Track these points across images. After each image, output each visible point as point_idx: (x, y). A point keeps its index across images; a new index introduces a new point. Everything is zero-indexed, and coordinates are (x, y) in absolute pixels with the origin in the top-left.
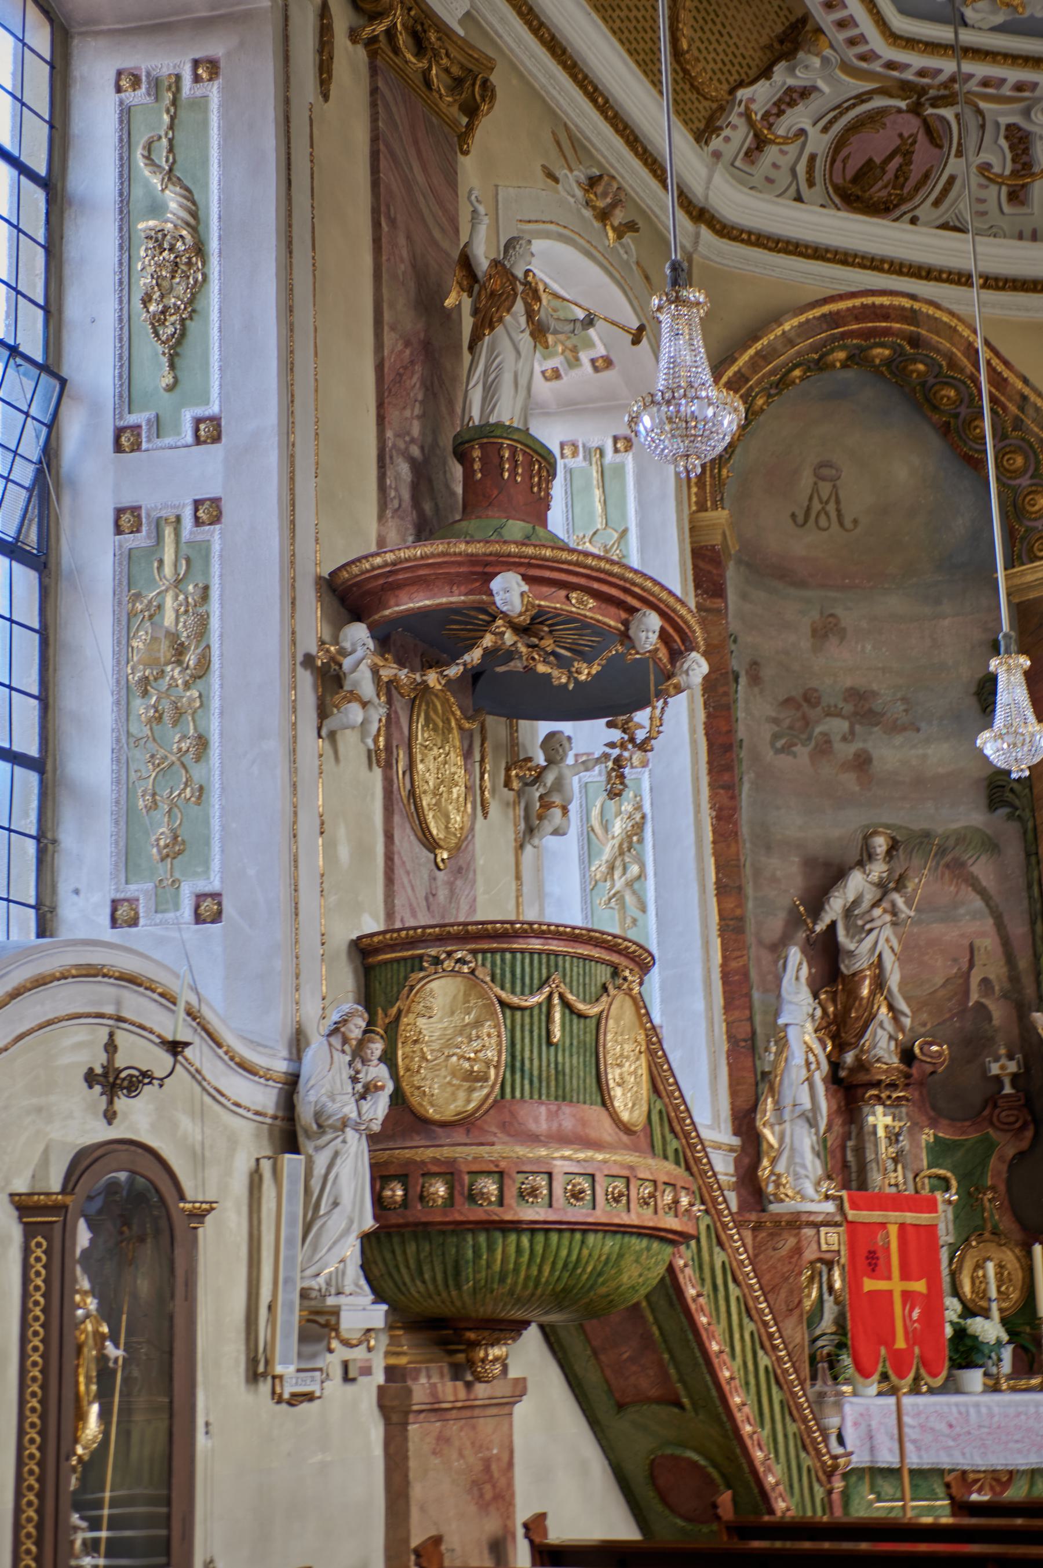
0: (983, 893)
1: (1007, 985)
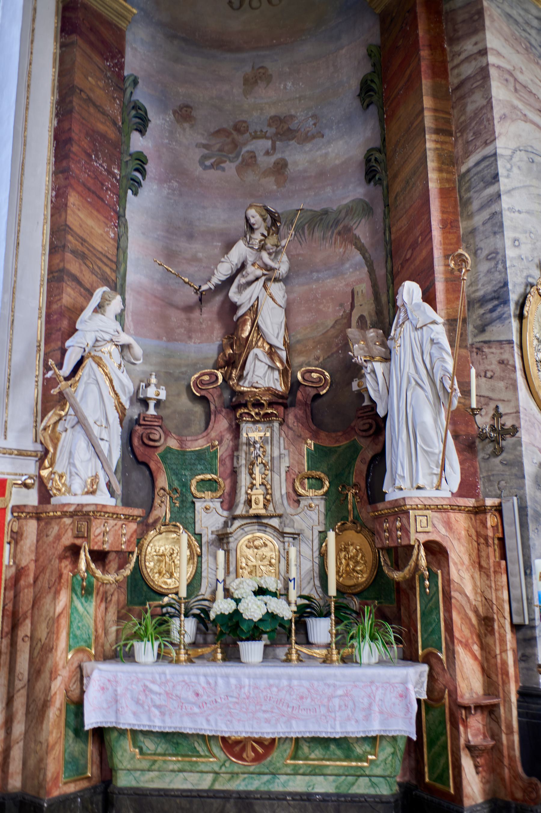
0: (362, 249)
1: (375, 318)
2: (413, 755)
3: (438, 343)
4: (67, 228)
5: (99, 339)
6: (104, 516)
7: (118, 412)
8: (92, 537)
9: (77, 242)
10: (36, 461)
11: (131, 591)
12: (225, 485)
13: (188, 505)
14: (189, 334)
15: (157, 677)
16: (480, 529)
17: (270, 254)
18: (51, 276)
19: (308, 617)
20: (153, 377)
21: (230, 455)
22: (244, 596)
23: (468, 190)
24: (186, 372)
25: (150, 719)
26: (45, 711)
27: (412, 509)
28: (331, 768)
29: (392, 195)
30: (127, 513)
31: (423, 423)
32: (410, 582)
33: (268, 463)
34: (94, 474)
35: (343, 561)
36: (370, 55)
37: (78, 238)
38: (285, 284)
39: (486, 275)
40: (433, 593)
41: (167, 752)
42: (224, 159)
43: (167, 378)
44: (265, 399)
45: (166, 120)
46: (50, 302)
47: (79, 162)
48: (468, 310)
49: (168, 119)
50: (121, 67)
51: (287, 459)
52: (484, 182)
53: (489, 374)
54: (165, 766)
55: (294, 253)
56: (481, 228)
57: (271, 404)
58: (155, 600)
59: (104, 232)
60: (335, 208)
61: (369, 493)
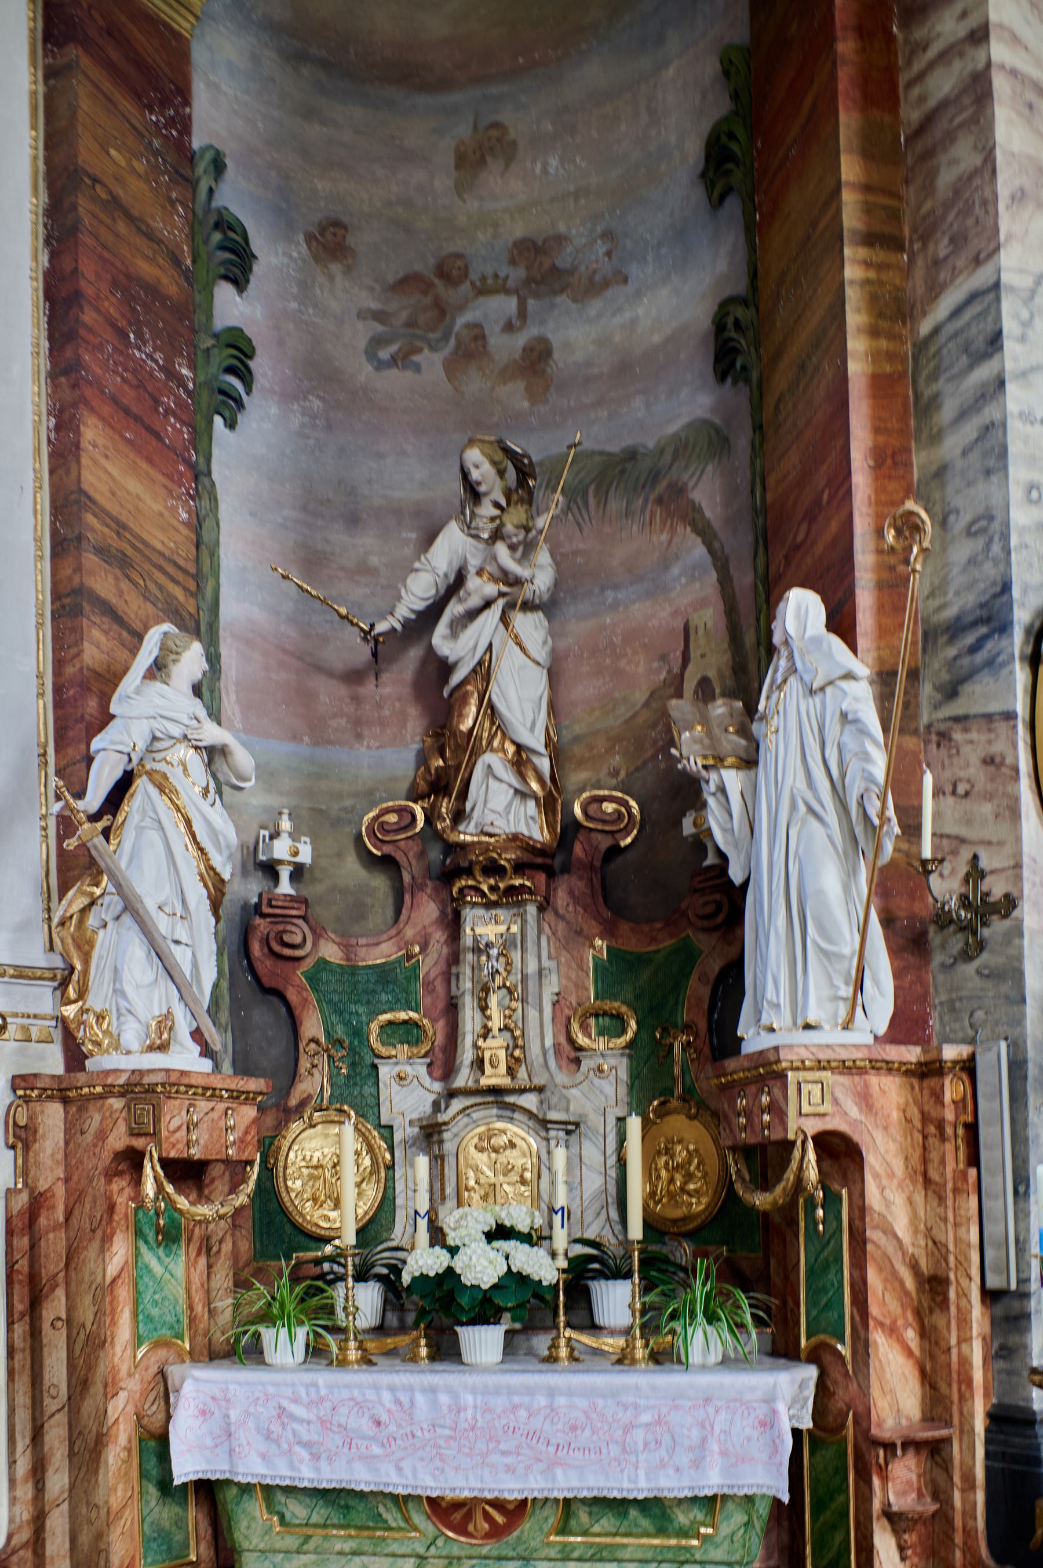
0: (705, 532)
1: (730, 682)
2: (785, 1524)
3: (856, 721)
4: (83, 499)
5: (158, 734)
6: (187, 1092)
7: (206, 886)
8: (164, 1134)
9: (106, 530)
10: (55, 989)
11: (261, 1234)
12: (436, 1031)
13: (365, 1071)
14: (358, 728)
15: (303, 1392)
16: (929, 1106)
17: (512, 548)
18: (58, 604)
19: (593, 1278)
20: (285, 817)
21: (443, 973)
22: (466, 1241)
23: (934, 377)
24: (353, 808)
25: (292, 1466)
26: (100, 1452)
27: (792, 1069)
28: (630, 1549)
29: (770, 401)
30: (233, 1087)
31: (820, 892)
32: (788, 1211)
33: (516, 986)
34: (165, 1011)
35: (664, 1173)
36: (726, 73)
37: (108, 520)
38: (549, 616)
39: (964, 570)
40: (831, 1232)
41: (329, 1522)
42: (419, 344)
43: (313, 820)
44: (507, 858)
45: (291, 257)
46: (59, 661)
47: (100, 348)
48: (924, 650)
49: (295, 255)
50: (185, 126)
51: (554, 978)
52: (969, 355)
53: (961, 789)
54: (326, 1545)
55: (566, 548)
56: (959, 464)
57: (519, 868)
58: (308, 1249)
59: (166, 508)
60: (651, 444)
61: (715, 1041)
